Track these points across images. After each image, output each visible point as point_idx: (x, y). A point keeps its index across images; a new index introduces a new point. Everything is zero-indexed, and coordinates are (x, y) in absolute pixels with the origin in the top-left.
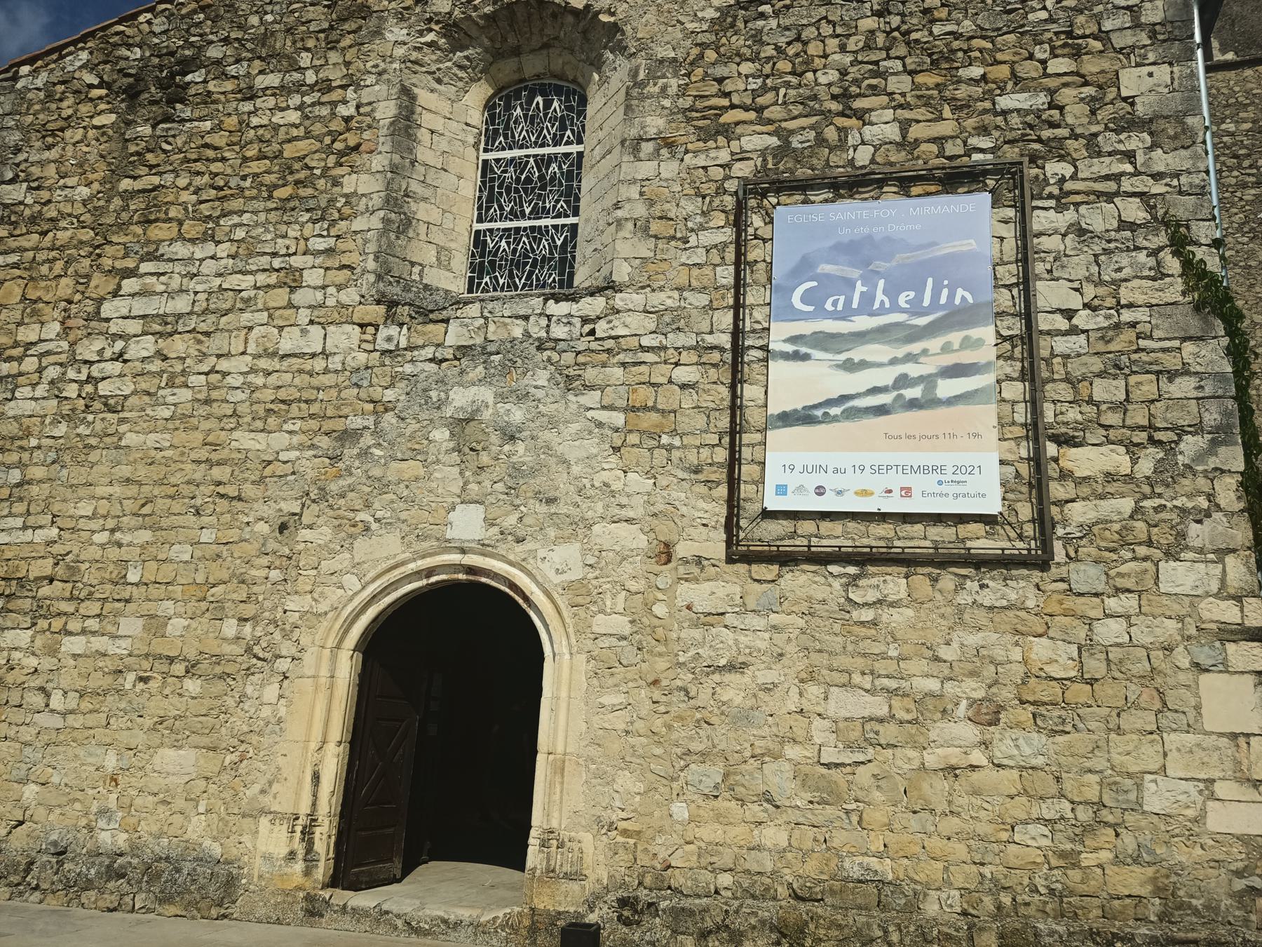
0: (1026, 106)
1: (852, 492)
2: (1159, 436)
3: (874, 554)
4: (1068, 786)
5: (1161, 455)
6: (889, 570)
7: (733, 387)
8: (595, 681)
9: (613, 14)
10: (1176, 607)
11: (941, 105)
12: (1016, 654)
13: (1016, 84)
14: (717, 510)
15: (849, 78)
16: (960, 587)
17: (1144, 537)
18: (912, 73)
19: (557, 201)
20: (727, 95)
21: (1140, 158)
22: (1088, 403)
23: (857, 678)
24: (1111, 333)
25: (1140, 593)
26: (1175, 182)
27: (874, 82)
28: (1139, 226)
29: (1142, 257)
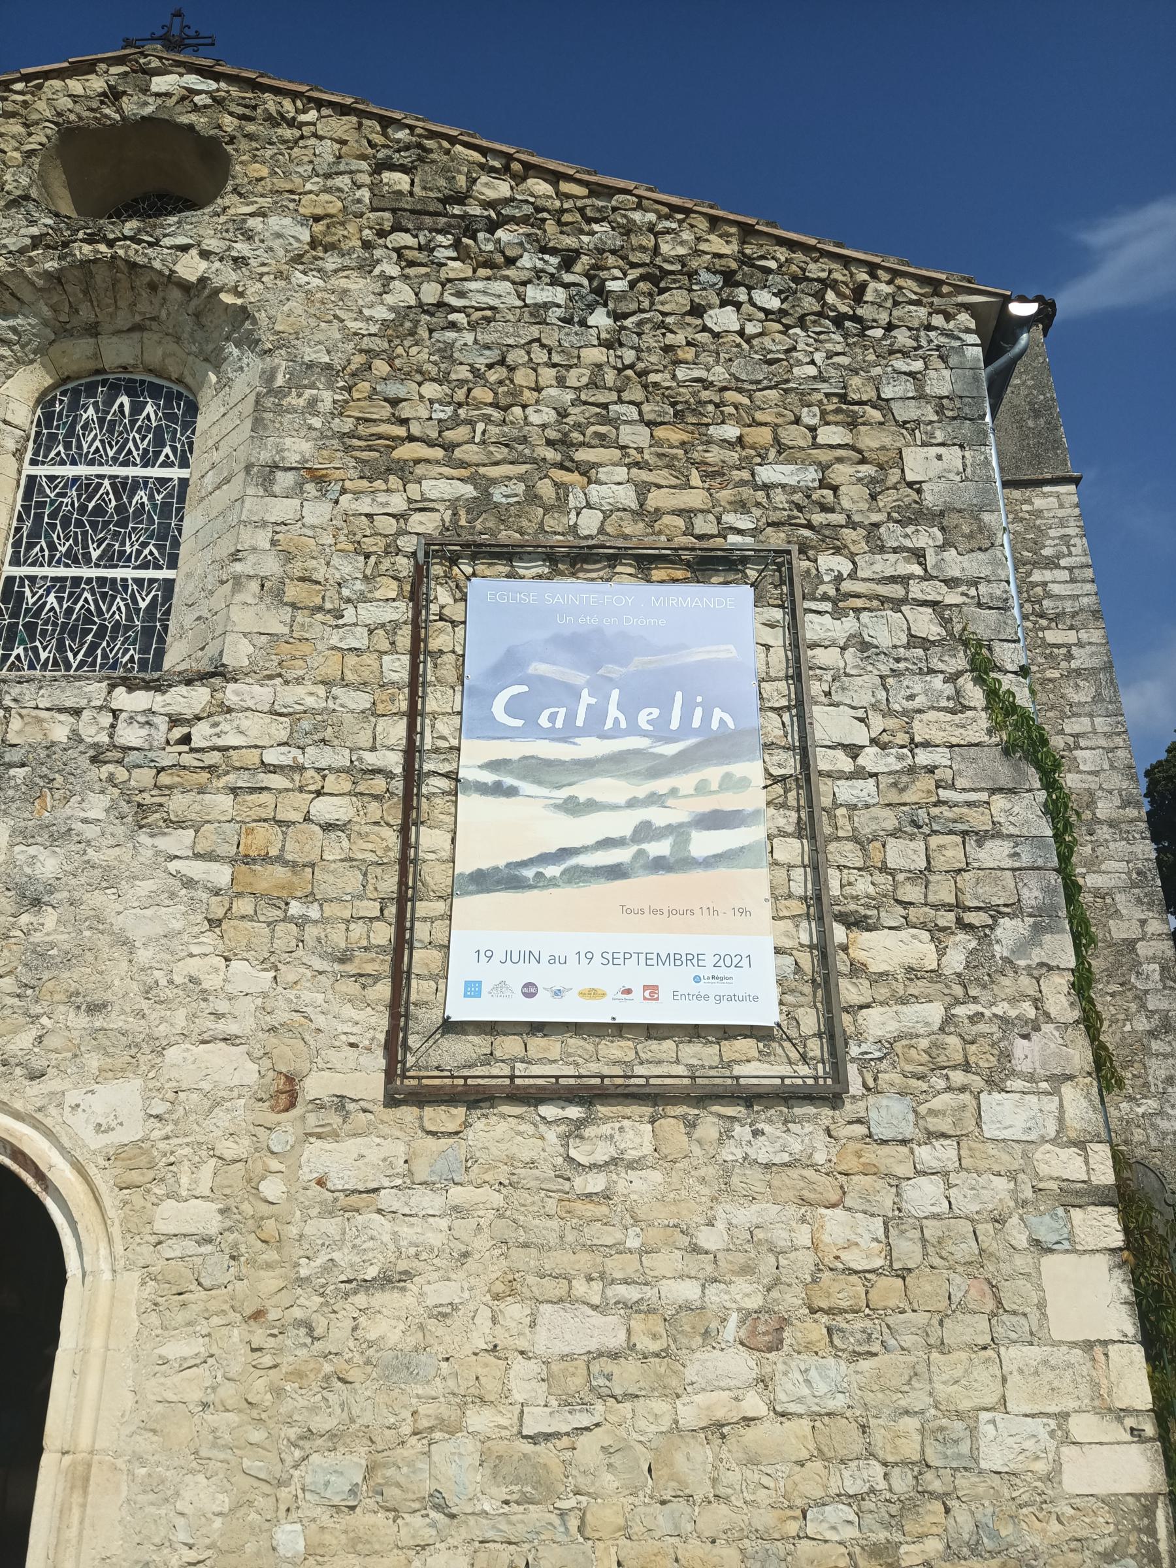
0: (792, 481)
1: (575, 992)
2: (970, 918)
3: (607, 1087)
4: (879, 1437)
5: (974, 944)
6: (627, 1110)
7: (404, 831)
8: (154, 1319)
9: (241, 295)
10: (1005, 1158)
11: (688, 469)
12: (803, 1236)
13: (779, 453)
14: (373, 1020)
15: (569, 420)
16: (725, 1136)
17: (958, 1058)
18: (649, 424)
19: (144, 545)
20: (404, 422)
21: (931, 559)
22: (881, 870)
23: (580, 1288)
24: (905, 779)
25: (959, 1139)
26: (973, 592)
27: (602, 429)
28: (933, 642)
29: (937, 682)
